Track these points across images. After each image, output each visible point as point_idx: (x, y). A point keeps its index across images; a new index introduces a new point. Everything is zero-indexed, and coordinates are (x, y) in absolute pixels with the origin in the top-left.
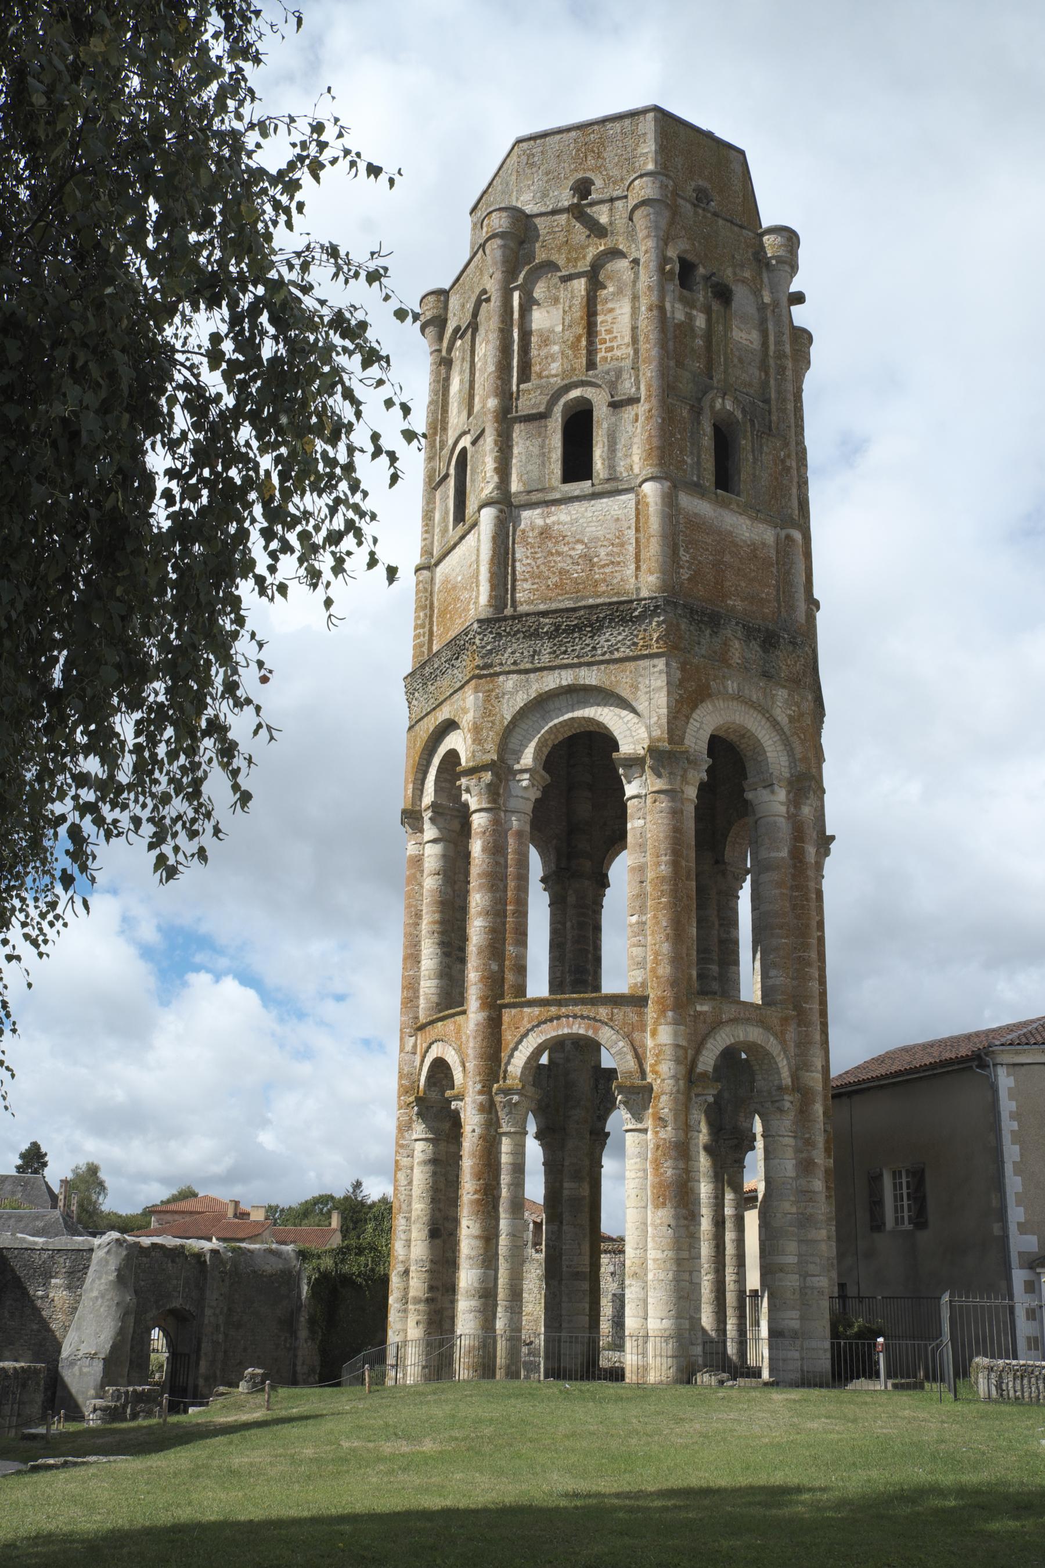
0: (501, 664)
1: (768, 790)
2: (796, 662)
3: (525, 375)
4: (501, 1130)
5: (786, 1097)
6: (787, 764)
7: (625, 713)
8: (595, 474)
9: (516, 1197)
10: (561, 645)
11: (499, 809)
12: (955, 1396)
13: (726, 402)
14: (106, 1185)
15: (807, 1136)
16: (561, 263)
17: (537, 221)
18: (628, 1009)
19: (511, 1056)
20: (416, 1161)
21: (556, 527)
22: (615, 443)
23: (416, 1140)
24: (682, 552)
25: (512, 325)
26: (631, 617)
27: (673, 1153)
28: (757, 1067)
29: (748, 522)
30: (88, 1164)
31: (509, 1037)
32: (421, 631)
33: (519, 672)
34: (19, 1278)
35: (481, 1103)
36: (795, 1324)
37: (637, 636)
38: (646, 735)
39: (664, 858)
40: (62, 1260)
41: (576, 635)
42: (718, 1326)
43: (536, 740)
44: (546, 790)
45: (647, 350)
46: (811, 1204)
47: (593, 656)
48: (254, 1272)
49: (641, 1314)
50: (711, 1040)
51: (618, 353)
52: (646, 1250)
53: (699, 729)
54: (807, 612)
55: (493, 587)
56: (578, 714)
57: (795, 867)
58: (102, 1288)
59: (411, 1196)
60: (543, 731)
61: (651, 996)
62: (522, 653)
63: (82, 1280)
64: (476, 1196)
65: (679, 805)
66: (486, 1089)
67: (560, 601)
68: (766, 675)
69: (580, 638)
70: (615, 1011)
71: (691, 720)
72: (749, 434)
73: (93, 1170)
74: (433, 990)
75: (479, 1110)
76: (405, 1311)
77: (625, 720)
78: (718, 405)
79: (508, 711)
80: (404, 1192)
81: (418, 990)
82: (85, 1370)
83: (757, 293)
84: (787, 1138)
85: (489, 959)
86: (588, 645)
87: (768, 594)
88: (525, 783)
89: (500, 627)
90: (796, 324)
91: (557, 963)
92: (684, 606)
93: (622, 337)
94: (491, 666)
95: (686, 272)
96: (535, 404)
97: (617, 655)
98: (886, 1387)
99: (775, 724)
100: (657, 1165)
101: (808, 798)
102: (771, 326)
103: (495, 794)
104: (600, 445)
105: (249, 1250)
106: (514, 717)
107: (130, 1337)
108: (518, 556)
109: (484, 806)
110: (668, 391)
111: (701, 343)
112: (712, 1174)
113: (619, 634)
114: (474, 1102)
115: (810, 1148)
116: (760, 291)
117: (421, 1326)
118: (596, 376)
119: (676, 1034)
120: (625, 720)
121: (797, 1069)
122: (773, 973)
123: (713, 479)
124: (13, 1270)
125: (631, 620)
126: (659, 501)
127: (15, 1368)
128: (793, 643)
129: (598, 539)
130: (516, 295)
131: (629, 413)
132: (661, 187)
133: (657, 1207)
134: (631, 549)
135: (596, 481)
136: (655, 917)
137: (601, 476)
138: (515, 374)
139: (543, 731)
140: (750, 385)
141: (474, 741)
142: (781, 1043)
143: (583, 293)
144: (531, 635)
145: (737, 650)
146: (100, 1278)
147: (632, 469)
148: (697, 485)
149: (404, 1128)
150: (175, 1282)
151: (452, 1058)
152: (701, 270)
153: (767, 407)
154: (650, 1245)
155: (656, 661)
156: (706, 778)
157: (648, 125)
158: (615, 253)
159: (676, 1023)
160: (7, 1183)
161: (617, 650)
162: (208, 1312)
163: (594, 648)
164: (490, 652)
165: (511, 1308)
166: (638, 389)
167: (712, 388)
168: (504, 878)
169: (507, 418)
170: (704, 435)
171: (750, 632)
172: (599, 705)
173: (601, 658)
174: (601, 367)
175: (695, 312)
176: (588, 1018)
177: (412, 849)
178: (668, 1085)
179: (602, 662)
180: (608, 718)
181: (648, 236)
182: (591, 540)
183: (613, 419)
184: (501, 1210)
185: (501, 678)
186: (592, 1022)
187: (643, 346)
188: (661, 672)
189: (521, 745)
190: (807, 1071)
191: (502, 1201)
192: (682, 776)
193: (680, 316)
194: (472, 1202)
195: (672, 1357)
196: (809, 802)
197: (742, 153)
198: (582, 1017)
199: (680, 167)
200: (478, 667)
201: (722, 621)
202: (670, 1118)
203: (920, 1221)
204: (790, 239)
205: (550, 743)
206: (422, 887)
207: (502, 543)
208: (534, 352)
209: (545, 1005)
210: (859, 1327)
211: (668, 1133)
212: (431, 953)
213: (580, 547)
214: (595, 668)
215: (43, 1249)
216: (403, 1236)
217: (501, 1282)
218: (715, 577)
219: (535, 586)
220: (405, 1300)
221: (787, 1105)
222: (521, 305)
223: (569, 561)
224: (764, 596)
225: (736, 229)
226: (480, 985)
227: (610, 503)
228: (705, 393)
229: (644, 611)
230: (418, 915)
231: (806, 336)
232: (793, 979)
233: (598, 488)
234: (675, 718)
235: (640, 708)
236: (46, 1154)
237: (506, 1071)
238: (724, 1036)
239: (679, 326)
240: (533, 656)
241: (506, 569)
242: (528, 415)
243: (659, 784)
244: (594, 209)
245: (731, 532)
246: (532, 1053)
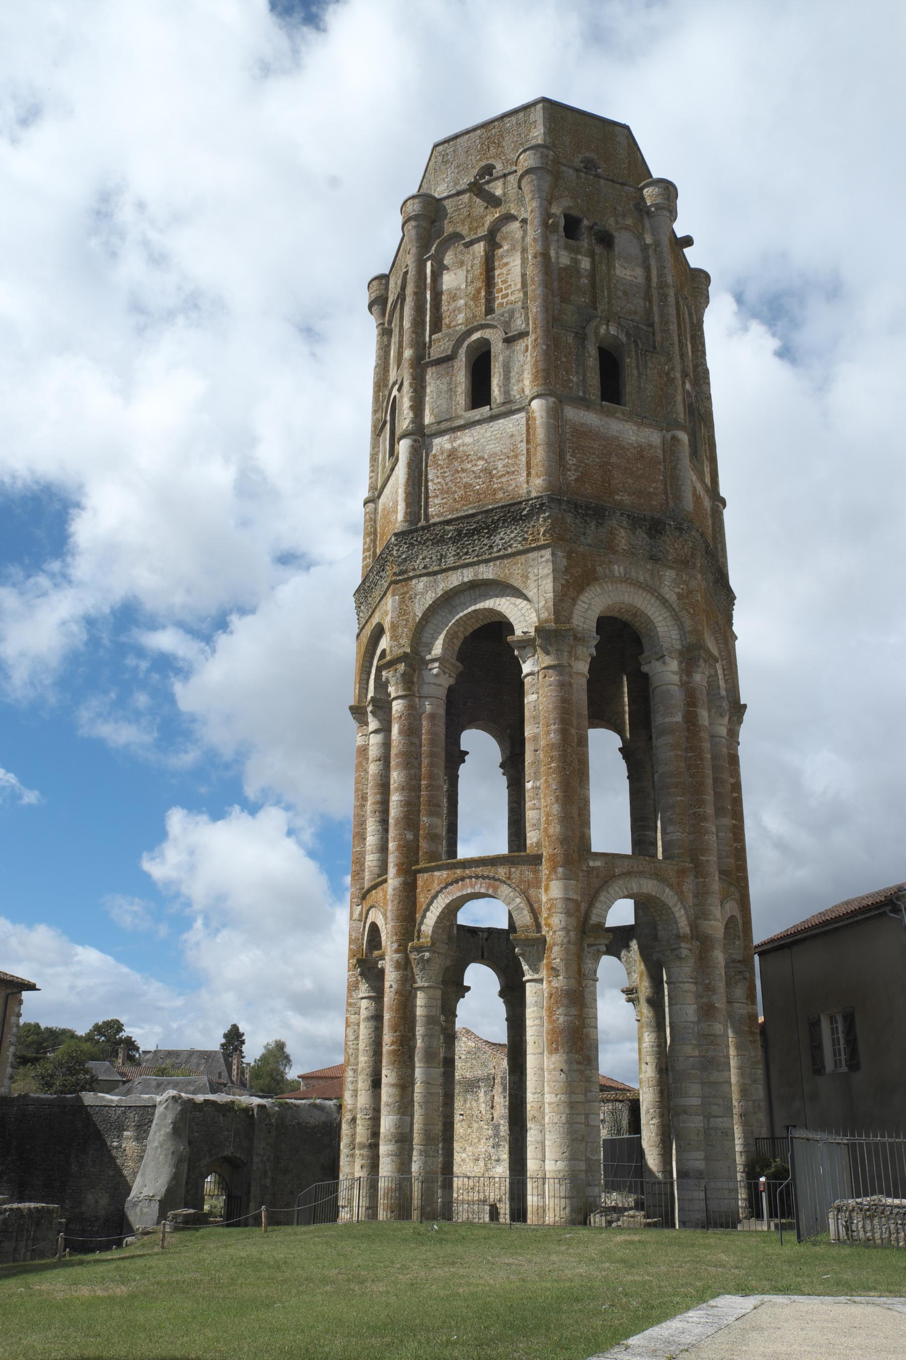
0: (414, 569)
1: (660, 661)
2: (683, 546)
3: (437, 326)
4: (416, 985)
5: (683, 945)
6: (678, 637)
7: (519, 601)
8: (493, 400)
9: (429, 1047)
10: (463, 548)
11: (413, 695)
12: (799, 1237)
13: (611, 328)
14: (291, 1058)
15: (707, 981)
16: (464, 233)
17: (445, 203)
18: (524, 868)
19: (424, 916)
20: (362, 1017)
21: (461, 449)
22: (510, 372)
23: (362, 998)
24: (568, 457)
25: (425, 289)
26: (521, 516)
27: (565, 1001)
28: (658, 918)
29: (635, 428)
30: (276, 1041)
31: (422, 899)
32: (367, 554)
33: (428, 574)
34: (99, 1131)
35: (397, 961)
36: (700, 1165)
37: (527, 532)
38: (536, 619)
39: (553, 727)
40: (132, 1115)
41: (476, 537)
42: (664, 1167)
43: (445, 632)
44: (461, 678)
45: (533, 291)
46: (713, 1047)
47: (490, 554)
48: (299, 1124)
49: (540, 1156)
50: (605, 893)
51: (512, 298)
52: (543, 1094)
53: (587, 610)
54: (712, 508)
55: (408, 505)
56: (480, 606)
57: (688, 730)
58: (161, 1139)
59: (358, 1049)
60: (450, 624)
61: (544, 854)
62: (431, 558)
63: (147, 1132)
64: (393, 1047)
65: (567, 678)
66: (402, 948)
67: (465, 511)
68: (653, 558)
69: (479, 540)
70: (513, 870)
71: (579, 602)
72: (633, 353)
73: (280, 1046)
74: (375, 863)
75: (395, 967)
76: (353, 1156)
77: (520, 607)
78: (603, 330)
79: (418, 610)
80: (352, 1047)
81: (364, 864)
82: (145, 1210)
83: (640, 237)
84: (687, 985)
85: (405, 829)
86: (485, 545)
87: (655, 488)
88: (435, 671)
89: (412, 538)
90: (692, 266)
91: (514, 838)
92: (568, 502)
93: (516, 285)
94: (406, 572)
95: (572, 227)
96: (444, 350)
97: (510, 550)
98: (769, 1227)
99: (664, 602)
100: (551, 1013)
101: (698, 667)
102: (653, 263)
103: (409, 682)
104: (497, 375)
105: (295, 1105)
106: (424, 614)
107: (184, 1182)
108: (430, 477)
109: (400, 693)
110: (553, 323)
111: (586, 281)
112: (655, 1024)
113: (512, 532)
114: (391, 960)
115: (710, 993)
116: (642, 234)
117: (365, 1170)
118: (493, 319)
119: (566, 889)
120: (520, 607)
121: (697, 918)
122: (670, 829)
123: (599, 393)
124: (95, 1125)
125: (521, 519)
126: (544, 414)
127: (29, 1209)
128: (680, 529)
129: (496, 454)
130: (429, 264)
131: (520, 345)
132: (541, 157)
133: (550, 1053)
134: (524, 459)
135: (493, 406)
136: (546, 781)
137: (498, 401)
138: (428, 328)
139: (450, 624)
140: (635, 313)
141: (391, 638)
142: (677, 894)
143: (482, 253)
144: (438, 542)
145: (623, 538)
146: (160, 1130)
147: (523, 392)
148: (583, 399)
149: (353, 987)
150: (226, 1133)
151: (380, 923)
152: (586, 222)
153: (650, 329)
154: (546, 1089)
155: (543, 552)
156: (595, 653)
157: (538, 114)
158: (509, 218)
159: (566, 878)
160: (194, 1057)
161: (510, 546)
162: (256, 1159)
163: (491, 547)
164: (405, 560)
165: (425, 1151)
166: (528, 324)
167: (596, 317)
168: (418, 757)
169: (420, 365)
170: (589, 356)
171: (635, 521)
172: (497, 596)
173: (496, 555)
174: (498, 311)
175: (580, 257)
176: (488, 877)
177: (360, 741)
178: (560, 937)
179: (497, 558)
180: (505, 607)
181: (532, 199)
182: (490, 456)
183: (508, 352)
184: (416, 1059)
185: (414, 582)
186: (492, 882)
187: (530, 288)
188: (547, 561)
189: (433, 638)
190: (705, 920)
191: (417, 1051)
192: (569, 652)
193: (565, 259)
194: (389, 1052)
195: (565, 1198)
196: (700, 670)
197: (627, 128)
198: (483, 877)
199: (567, 144)
200: (395, 574)
201: (607, 513)
202: (562, 968)
203: (854, 1064)
204: (667, 189)
205: (461, 636)
206: (367, 772)
207: (417, 467)
208: (444, 308)
209: (452, 868)
210: (776, 1166)
211: (560, 982)
212: (374, 830)
213: (481, 463)
214: (491, 564)
215: (117, 1106)
216: (350, 1087)
217: (416, 1127)
218: (602, 477)
219: (444, 501)
220: (352, 1146)
221: (685, 952)
222: (432, 272)
223: (473, 476)
224: (651, 490)
225: (618, 186)
226: (397, 854)
227: (506, 423)
228: (589, 321)
229: (532, 510)
230: (364, 798)
231: (702, 275)
232: (689, 834)
233: (495, 411)
234: (561, 600)
235: (530, 595)
236: (243, 1034)
237: (419, 931)
238: (617, 889)
239: (566, 268)
240: (440, 560)
241: (420, 489)
242: (438, 359)
243: (547, 661)
244: (491, 185)
245: (617, 438)
246: (442, 912)
